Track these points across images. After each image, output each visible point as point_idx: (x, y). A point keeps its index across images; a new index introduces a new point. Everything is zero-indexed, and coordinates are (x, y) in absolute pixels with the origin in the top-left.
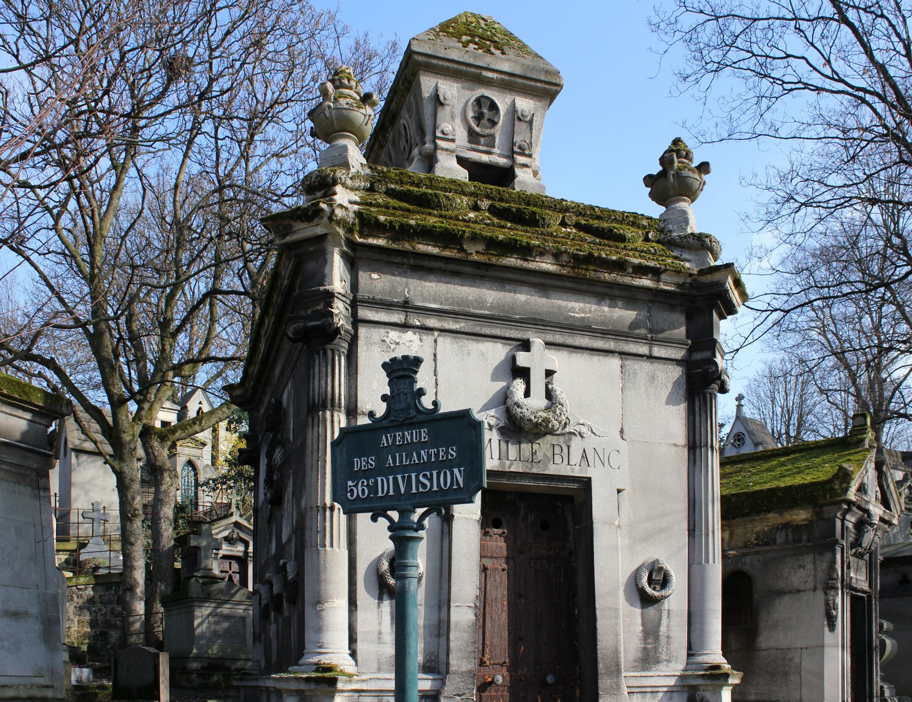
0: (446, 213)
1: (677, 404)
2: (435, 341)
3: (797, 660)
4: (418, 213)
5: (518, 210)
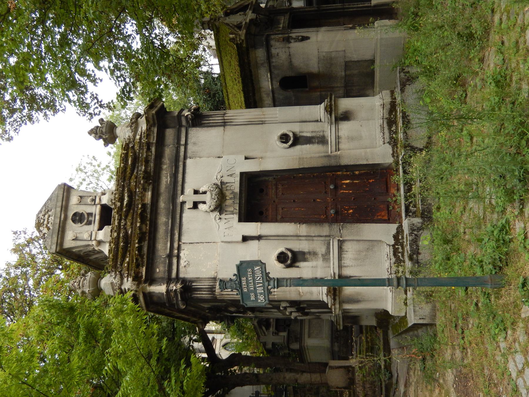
2: (184, 243)
3: (324, 54)
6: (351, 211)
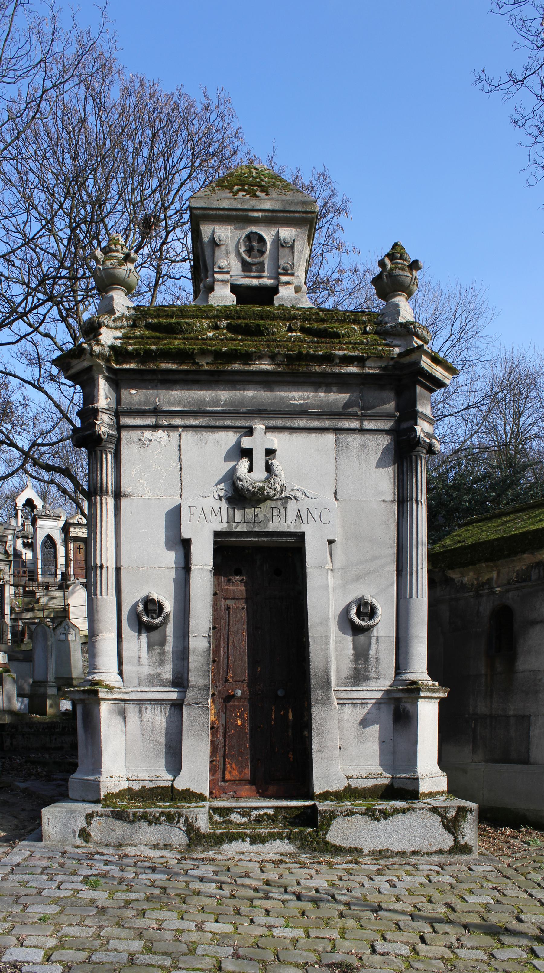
0: (189, 335)
1: (386, 467)
2: (180, 436)
4: (166, 339)
5: (247, 325)
6: (239, 722)
